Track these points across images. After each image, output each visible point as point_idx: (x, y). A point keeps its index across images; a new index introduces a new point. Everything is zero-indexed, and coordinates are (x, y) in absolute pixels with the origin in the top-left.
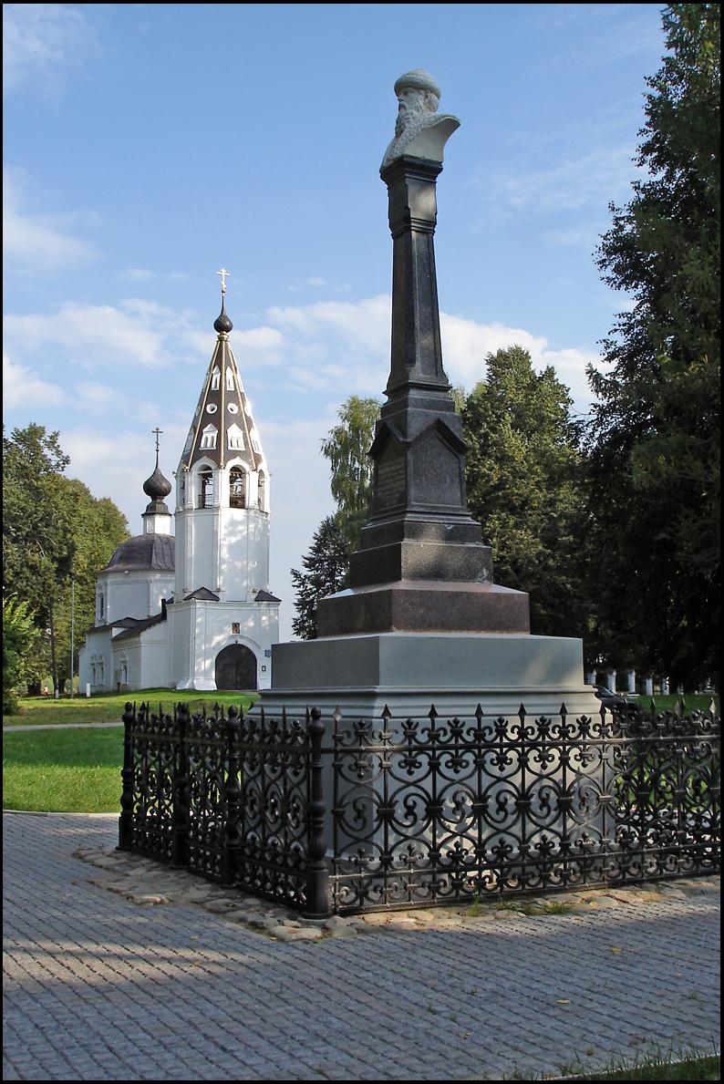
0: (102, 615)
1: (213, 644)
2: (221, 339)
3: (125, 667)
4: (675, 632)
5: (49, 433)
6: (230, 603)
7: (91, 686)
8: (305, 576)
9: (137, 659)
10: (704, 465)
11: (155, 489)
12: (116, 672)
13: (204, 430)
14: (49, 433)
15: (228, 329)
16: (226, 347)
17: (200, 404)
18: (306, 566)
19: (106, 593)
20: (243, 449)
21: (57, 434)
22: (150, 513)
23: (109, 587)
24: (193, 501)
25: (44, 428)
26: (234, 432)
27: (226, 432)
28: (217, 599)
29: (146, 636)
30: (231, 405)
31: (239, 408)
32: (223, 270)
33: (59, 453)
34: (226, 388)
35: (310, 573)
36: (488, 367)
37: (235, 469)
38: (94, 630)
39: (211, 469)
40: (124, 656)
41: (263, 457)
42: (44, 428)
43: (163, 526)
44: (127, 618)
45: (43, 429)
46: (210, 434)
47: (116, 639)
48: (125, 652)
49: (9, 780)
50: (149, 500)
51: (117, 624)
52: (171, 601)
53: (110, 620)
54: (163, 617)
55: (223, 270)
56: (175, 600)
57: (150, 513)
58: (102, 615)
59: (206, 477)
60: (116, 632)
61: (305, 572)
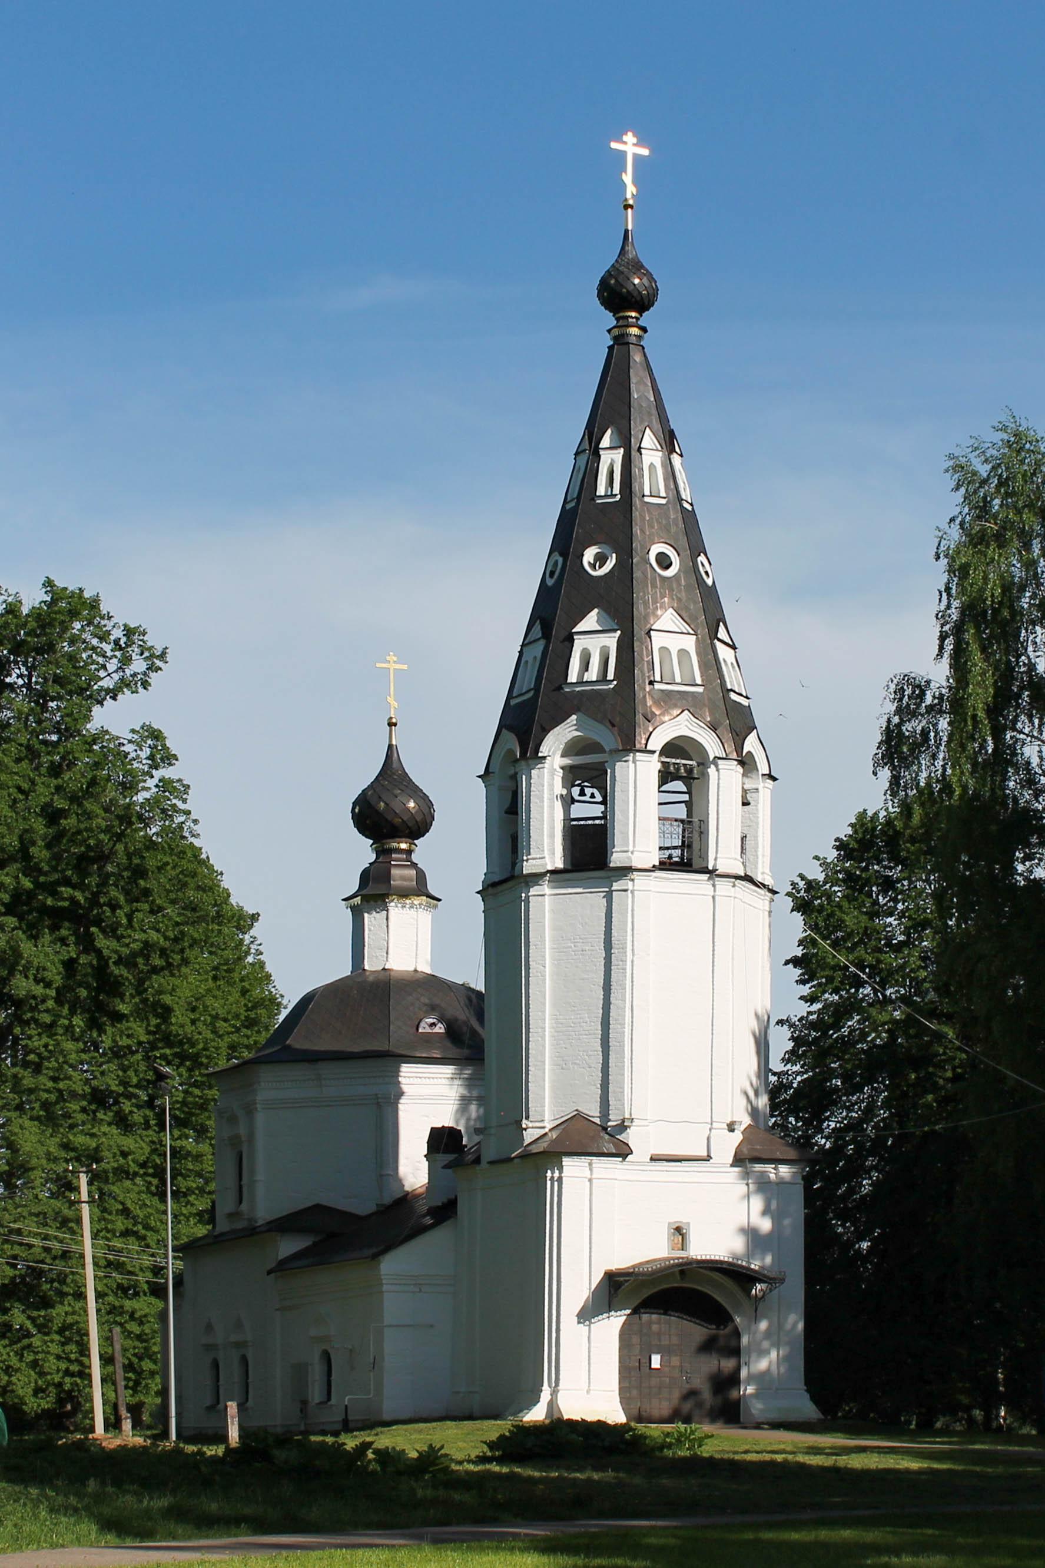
2: (620, 341)
4: (927, 985)
7: (92, 1429)
10: (565, 792)
11: (388, 816)
15: (643, 304)
22: (374, 891)
24: (547, 850)
25: (579, 1323)
26: (670, 636)
28: (623, 1152)
32: (630, 138)
37: (673, 748)
39: (603, 751)
41: (505, 750)
42: (579, 1323)
43: (410, 942)
46: (593, 645)
47: (283, 1267)
49: (69, 952)
50: (362, 852)
55: (630, 138)
57: (374, 891)
59: (590, 773)
60: (288, 1246)
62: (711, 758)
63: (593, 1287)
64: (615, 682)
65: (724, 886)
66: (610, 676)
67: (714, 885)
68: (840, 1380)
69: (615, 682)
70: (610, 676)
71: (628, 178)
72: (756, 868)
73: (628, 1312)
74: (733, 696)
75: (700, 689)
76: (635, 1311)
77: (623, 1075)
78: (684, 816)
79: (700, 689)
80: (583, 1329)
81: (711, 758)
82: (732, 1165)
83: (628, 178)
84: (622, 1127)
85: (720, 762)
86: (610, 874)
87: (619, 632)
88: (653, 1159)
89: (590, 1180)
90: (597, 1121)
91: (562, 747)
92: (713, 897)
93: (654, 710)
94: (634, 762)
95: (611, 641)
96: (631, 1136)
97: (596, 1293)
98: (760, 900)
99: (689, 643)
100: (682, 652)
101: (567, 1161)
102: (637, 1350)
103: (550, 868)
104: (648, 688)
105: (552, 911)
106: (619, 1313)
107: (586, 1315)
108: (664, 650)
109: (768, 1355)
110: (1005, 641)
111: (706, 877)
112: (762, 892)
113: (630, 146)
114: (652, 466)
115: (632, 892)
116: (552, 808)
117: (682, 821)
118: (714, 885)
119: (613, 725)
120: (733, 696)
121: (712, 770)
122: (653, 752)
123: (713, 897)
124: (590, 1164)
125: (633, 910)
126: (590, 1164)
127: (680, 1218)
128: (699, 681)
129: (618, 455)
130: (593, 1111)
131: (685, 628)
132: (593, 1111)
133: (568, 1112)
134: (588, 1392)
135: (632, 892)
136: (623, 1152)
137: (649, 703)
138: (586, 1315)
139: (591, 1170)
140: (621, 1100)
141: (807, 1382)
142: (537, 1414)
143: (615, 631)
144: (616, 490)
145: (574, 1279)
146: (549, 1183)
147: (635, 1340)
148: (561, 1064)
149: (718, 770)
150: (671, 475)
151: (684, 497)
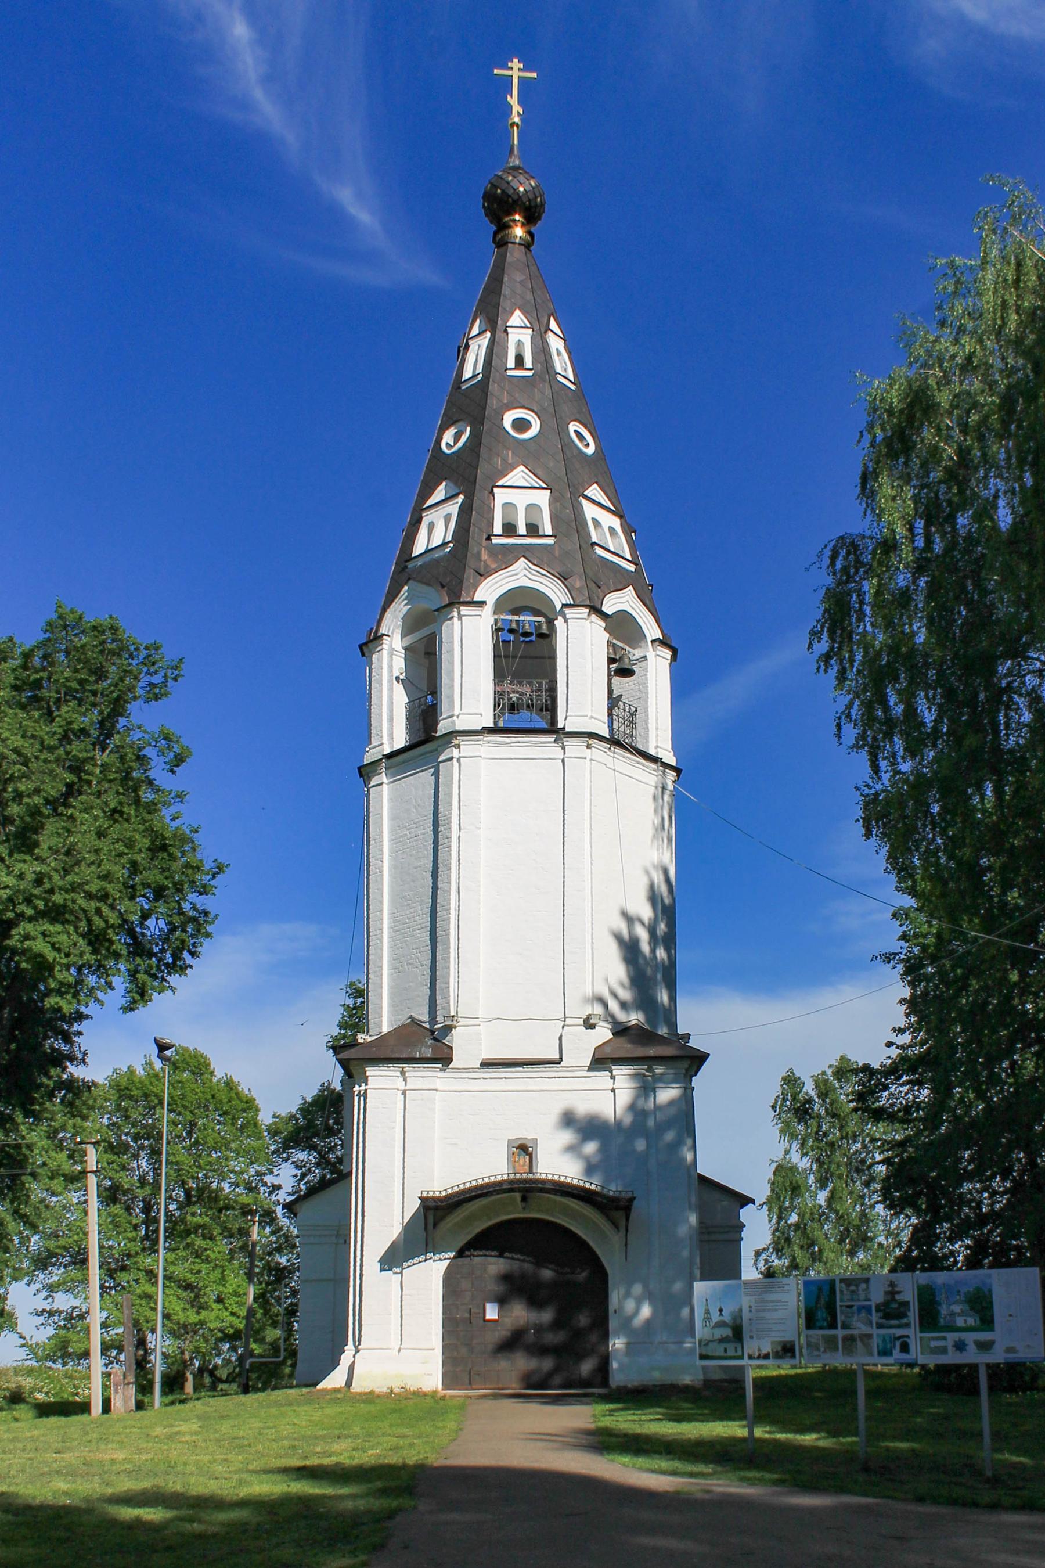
28: (443, 1058)
32: (516, 64)
37: (517, 601)
55: (516, 64)
62: (558, 607)
63: (406, 1221)
64: (451, 545)
65: (575, 748)
67: (563, 748)
69: (451, 545)
71: (513, 100)
72: (647, 741)
73: (452, 1255)
74: (599, 551)
75: (550, 541)
76: (460, 1254)
77: (449, 968)
79: (550, 541)
80: (392, 1278)
81: (558, 607)
82: (591, 1069)
83: (513, 100)
85: (567, 611)
86: (440, 742)
87: (462, 497)
88: (486, 1064)
89: (404, 1093)
90: (427, 1025)
91: (400, 623)
92: (563, 761)
93: (489, 563)
94: (460, 617)
96: (458, 1040)
97: (409, 1228)
98: (648, 777)
101: (370, 1071)
103: (387, 750)
104: (484, 543)
105: (391, 800)
106: (442, 1256)
107: (394, 1258)
111: (551, 738)
112: (653, 766)
113: (515, 70)
114: (519, 343)
115: (458, 760)
116: (391, 689)
118: (563, 748)
119: (443, 586)
120: (599, 551)
121: (559, 623)
122: (482, 604)
123: (563, 761)
124: (403, 1073)
126: (403, 1073)
127: (526, 1134)
128: (549, 531)
129: (485, 340)
130: (424, 1016)
131: (535, 482)
132: (424, 1016)
133: (403, 1019)
134: (399, 1351)
135: (458, 760)
136: (443, 1058)
137: (484, 556)
138: (394, 1258)
139: (405, 1080)
140: (446, 997)
143: (456, 495)
145: (382, 1212)
146: (356, 1099)
148: (397, 969)
149: (566, 621)
151: (559, 370)
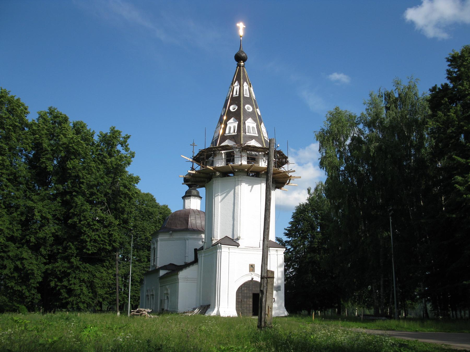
0: (154, 261)
1: (446, 157)
3: (168, 297)
5: (123, 135)
6: (247, 248)
8: (285, 241)
9: (175, 292)
12: (161, 301)
13: (229, 122)
14: (123, 135)
15: (244, 60)
16: (244, 72)
17: (225, 106)
18: (286, 234)
19: (157, 247)
20: (257, 135)
21: (129, 137)
23: (159, 243)
27: (244, 123)
28: (238, 245)
29: (182, 274)
30: (247, 106)
31: (253, 108)
33: (127, 149)
34: (243, 95)
35: (289, 239)
36: (449, 63)
38: (148, 273)
40: (167, 290)
44: (171, 264)
45: (119, 133)
48: (167, 287)
50: (187, 188)
51: (163, 268)
52: (202, 248)
53: (159, 265)
54: (196, 261)
56: (205, 247)
58: (154, 261)
60: (162, 273)
61: (285, 239)
66: (236, 131)
68: (293, 304)
70: (236, 131)
78: (260, 188)
84: (238, 239)
95: (236, 124)
96: (240, 242)
99: (255, 125)
100: (253, 128)
102: (240, 297)
108: (248, 126)
109: (277, 306)
110: (7, 237)
114: (246, 89)
117: (269, 278)
125: (201, 278)
127: (252, 263)
136: (238, 245)
141: (285, 306)
142: (214, 313)
144: (238, 94)
147: (240, 294)
150: (249, 91)
